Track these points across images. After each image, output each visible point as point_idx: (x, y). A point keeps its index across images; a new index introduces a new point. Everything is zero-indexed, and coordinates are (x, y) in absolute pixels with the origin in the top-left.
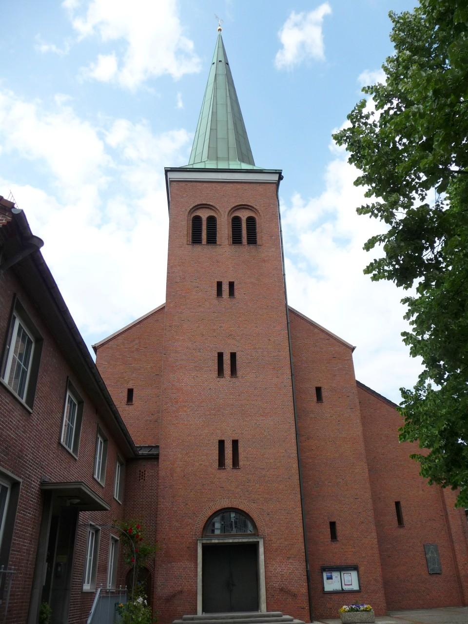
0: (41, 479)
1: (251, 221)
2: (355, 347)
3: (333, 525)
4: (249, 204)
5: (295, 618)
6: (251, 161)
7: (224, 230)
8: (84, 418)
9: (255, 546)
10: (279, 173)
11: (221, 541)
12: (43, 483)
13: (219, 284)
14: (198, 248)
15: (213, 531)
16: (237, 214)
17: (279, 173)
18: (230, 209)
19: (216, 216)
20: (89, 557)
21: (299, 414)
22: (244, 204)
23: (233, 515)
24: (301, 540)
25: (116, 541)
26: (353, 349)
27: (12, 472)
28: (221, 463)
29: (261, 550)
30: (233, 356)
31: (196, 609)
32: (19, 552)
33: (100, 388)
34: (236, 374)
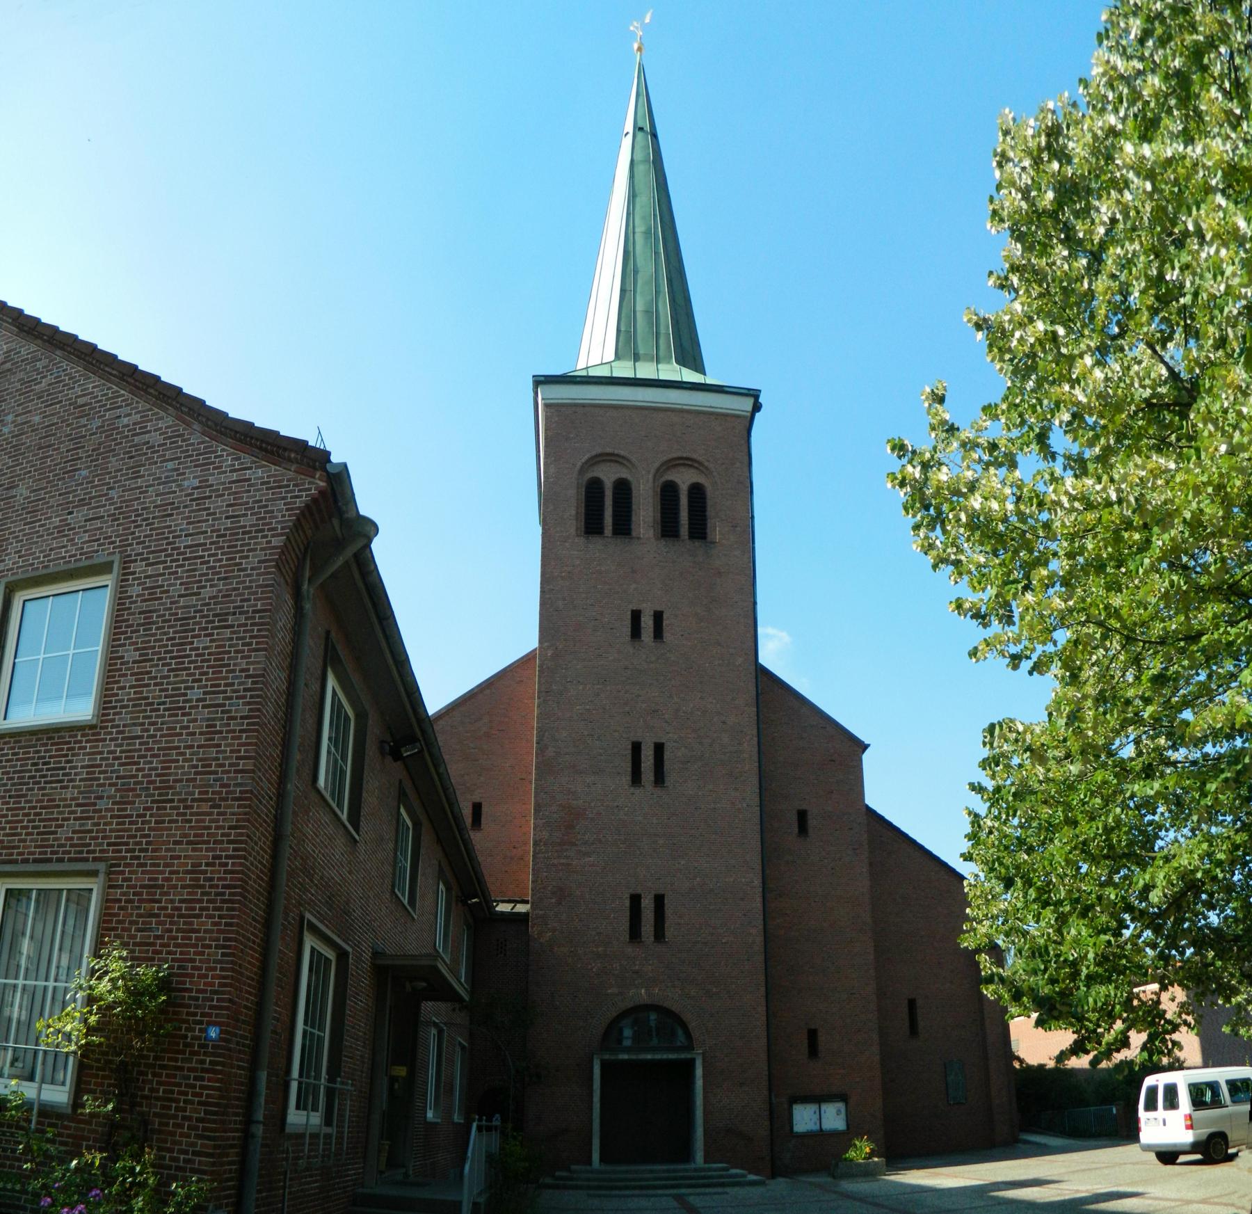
0: (372, 948)
1: (697, 492)
2: (869, 745)
3: (812, 1035)
4: (694, 456)
5: (750, 1173)
6: (699, 367)
7: (645, 512)
8: (422, 851)
9: (690, 1064)
10: (754, 395)
11: (634, 1057)
12: (376, 954)
13: (636, 616)
14: (596, 544)
15: (620, 1041)
16: (672, 476)
17: (754, 395)
18: (657, 465)
19: (629, 478)
20: (432, 1072)
21: (769, 855)
22: (685, 455)
23: (653, 1016)
24: (764, 1056)
25: (463, 1048)
26: (865, 747)
27: (339, 936)
28: (635, 933)
29: (699, 1072)
30: (659, 749)
31: (590, 1157)
32: (351, 1058)
33: (448, 800)
34: (663, 782)
